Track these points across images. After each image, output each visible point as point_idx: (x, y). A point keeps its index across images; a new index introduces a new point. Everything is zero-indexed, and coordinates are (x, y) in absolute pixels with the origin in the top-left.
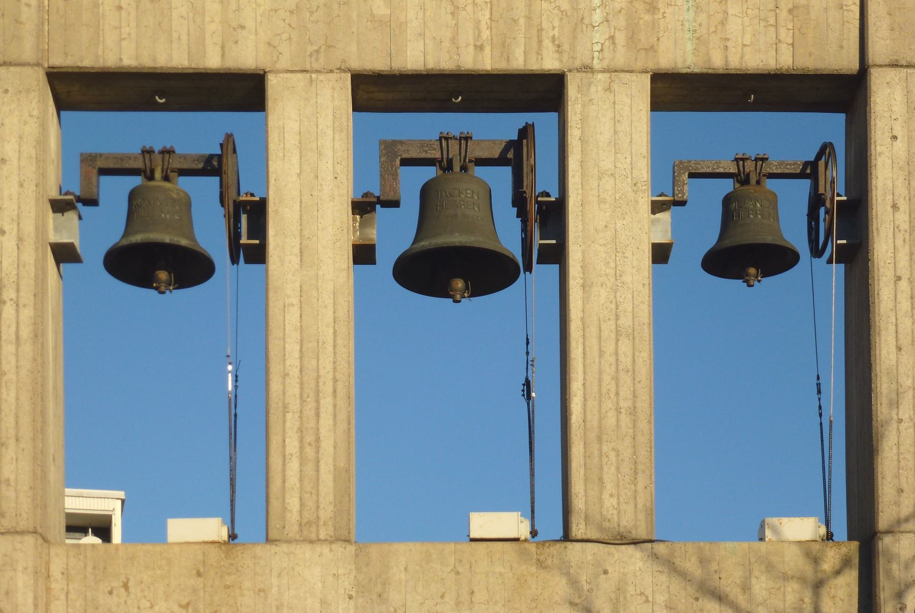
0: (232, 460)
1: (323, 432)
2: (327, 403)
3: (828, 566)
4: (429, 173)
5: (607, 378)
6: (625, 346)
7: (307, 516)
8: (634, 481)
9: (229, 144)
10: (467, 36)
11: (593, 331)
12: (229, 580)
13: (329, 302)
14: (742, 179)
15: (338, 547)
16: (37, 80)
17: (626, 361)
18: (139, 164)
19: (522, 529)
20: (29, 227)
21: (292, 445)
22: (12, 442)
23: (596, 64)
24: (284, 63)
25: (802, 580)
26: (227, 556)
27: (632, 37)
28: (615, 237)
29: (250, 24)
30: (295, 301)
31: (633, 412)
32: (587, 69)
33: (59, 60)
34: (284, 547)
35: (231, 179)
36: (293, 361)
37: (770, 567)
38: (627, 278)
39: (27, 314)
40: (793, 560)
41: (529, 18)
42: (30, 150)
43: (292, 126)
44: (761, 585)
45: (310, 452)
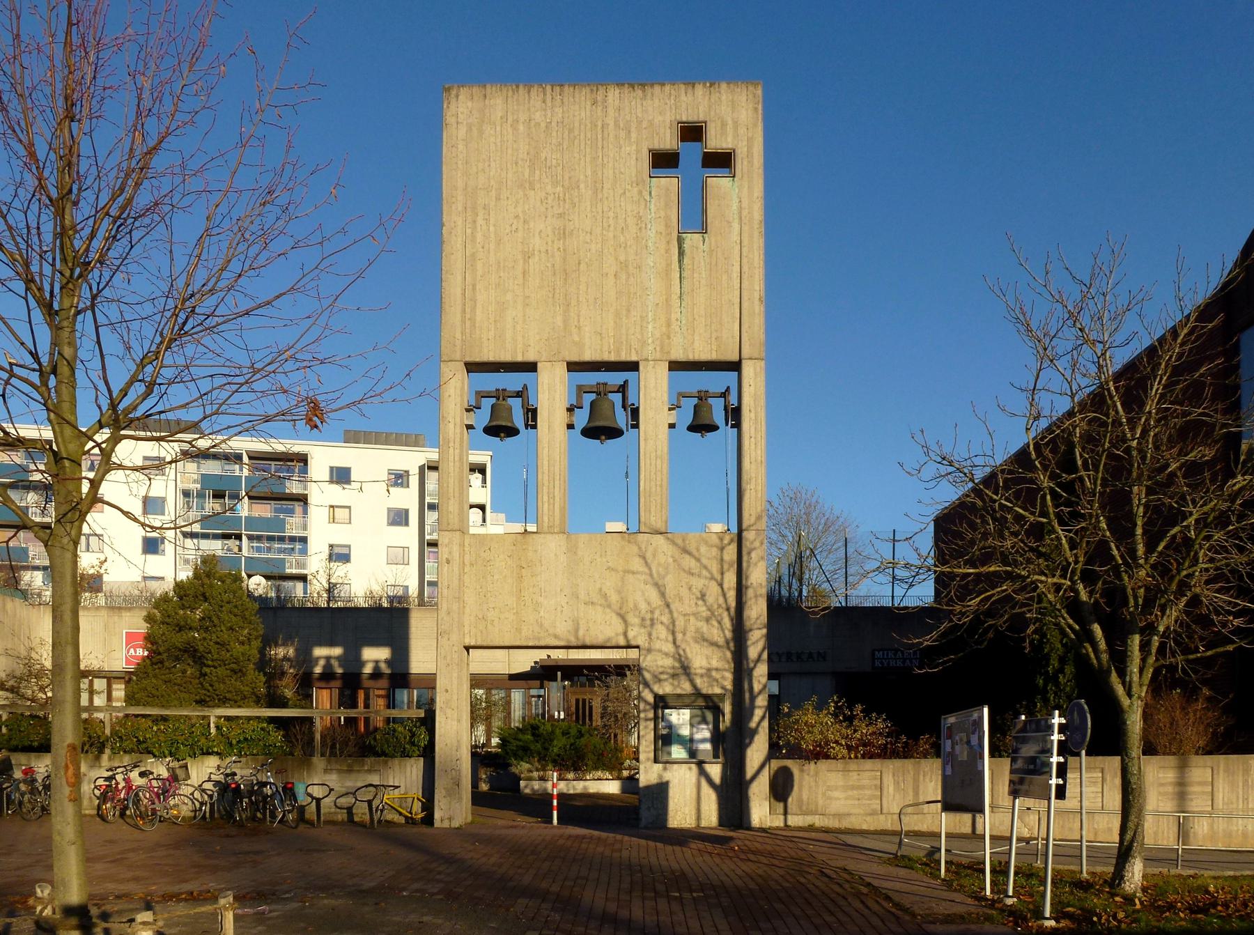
0: (526, 503)
1: (556, 494)
2: (557, 483)
3: (726, 542)
4: (593, 396)
5: (652, 474)
6: (659, 462)
7: (551, 524)
8: (661, 511)
9: (525, 387)
10: (606, 348)
11: (648, 455)
12: (524, 547)
13: (558, 445)
14: (700, 399)
15: (561, 535)
16: (463, 363)
17: (659, 467)
18: (495, 395)
19: (624, 529)
20: (458, 420)
21: (546, 498)
22: (452, 498)
23: (650, 358)
24: (542, 360)
25: (717, 547)
26: (524, 538)
27: (662, 348)
28: (656, 422)
29: (532, 345)
30: (547, 445)
31: (661, 486)
32: (647, 360)
33: (468, 359)
34: (543, 535)
35: (526, 399)
36: (546, 468)
37: (706, 543)
38: (660, 437)
39: (457, 451)
40: (715, 540)
41: (627, 341)
42: (458, 392)
43: (546, 381)
44: (703, 549)
45: (551, 501)
